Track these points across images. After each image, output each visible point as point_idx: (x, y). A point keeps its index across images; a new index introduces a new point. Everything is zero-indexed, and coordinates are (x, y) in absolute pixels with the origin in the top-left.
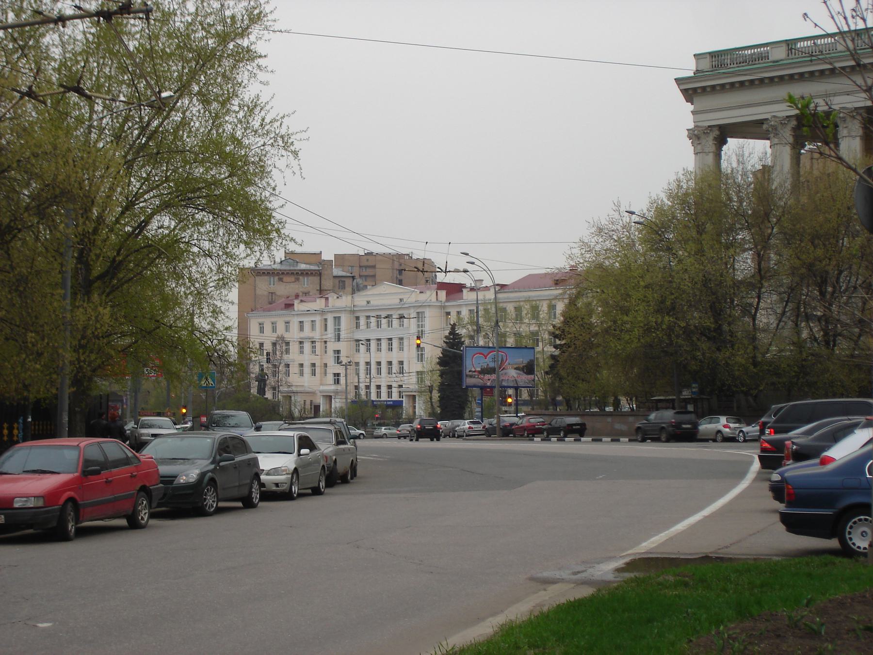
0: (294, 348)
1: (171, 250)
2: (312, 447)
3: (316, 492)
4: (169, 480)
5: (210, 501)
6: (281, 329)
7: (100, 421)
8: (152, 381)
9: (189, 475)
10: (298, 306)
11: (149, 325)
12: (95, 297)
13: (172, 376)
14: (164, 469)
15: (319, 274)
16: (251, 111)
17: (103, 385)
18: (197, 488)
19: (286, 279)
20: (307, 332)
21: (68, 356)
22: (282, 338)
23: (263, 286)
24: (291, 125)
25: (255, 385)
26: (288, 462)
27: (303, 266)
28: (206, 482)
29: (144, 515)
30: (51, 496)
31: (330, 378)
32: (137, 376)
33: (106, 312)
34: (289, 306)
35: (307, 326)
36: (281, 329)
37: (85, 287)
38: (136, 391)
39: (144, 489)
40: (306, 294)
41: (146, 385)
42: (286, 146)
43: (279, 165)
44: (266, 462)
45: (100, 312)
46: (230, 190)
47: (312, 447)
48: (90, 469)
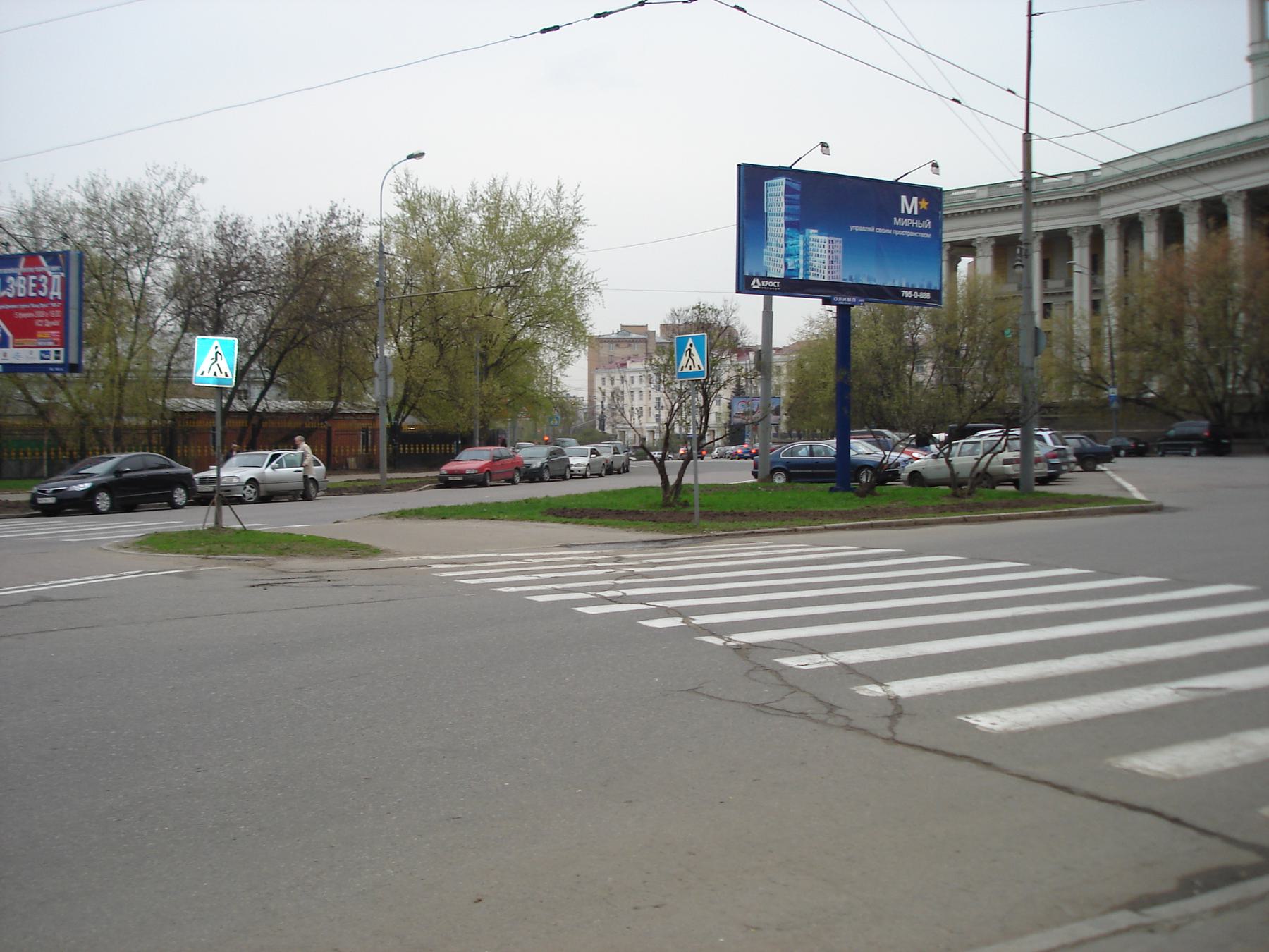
0: (627, 397)
1: (533, 346)
2: (598, 454)
3: (600, 476)
4: (528, 466)
5: (547, 476)
6: (617, 383)
7: (491, 440)
8: (523, 421)
9: (537, 464)
10: (630, 365)
11: (521, 390)
12: (491, 375)
13: (535, 419)
14: (526, 462)
15: (645, 341)
16: (575, 269)
17: (499, 425)
18: (540, 470)
19: (622, 345)
20: (637, 384)
21: (479, 409)
22: (618, 389)
23: (605, 351)
24: (598, 277)
25: (598, 422)
26: (585, 461)
27: (634, 336)
28: (544, 467)
29: (517, 479)
30: (480, 469)
31: (653, 419)
32: (514, 418)
33: (497, 386)
34: (624, 365)
35: (636, 380)
36: (617, 383)
37: (485, 371)
38: (514, 427)
39: (517, 468)
40: (636, 356)
41: (519, 424)
42: (595, 289)
43: (592, 296)
44: (573, 461)
45: (493, 386)
46: (561, 312)
47: (598, 454)
48: (495, 459)
